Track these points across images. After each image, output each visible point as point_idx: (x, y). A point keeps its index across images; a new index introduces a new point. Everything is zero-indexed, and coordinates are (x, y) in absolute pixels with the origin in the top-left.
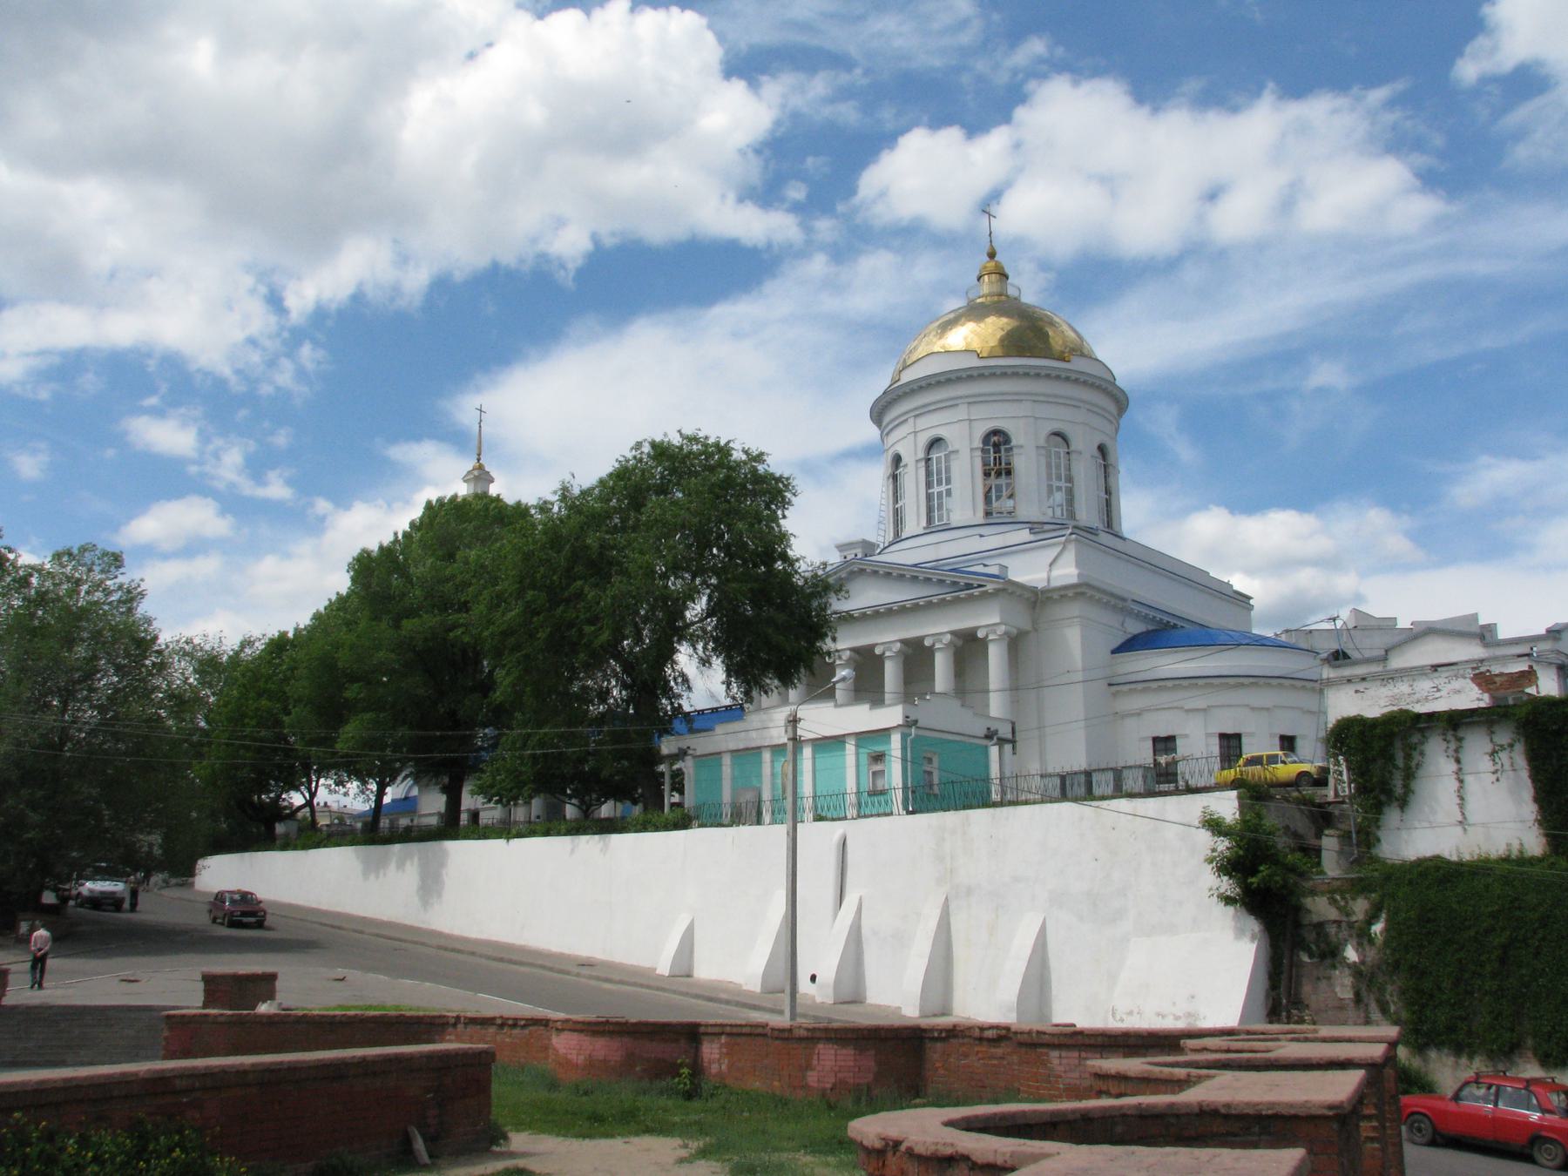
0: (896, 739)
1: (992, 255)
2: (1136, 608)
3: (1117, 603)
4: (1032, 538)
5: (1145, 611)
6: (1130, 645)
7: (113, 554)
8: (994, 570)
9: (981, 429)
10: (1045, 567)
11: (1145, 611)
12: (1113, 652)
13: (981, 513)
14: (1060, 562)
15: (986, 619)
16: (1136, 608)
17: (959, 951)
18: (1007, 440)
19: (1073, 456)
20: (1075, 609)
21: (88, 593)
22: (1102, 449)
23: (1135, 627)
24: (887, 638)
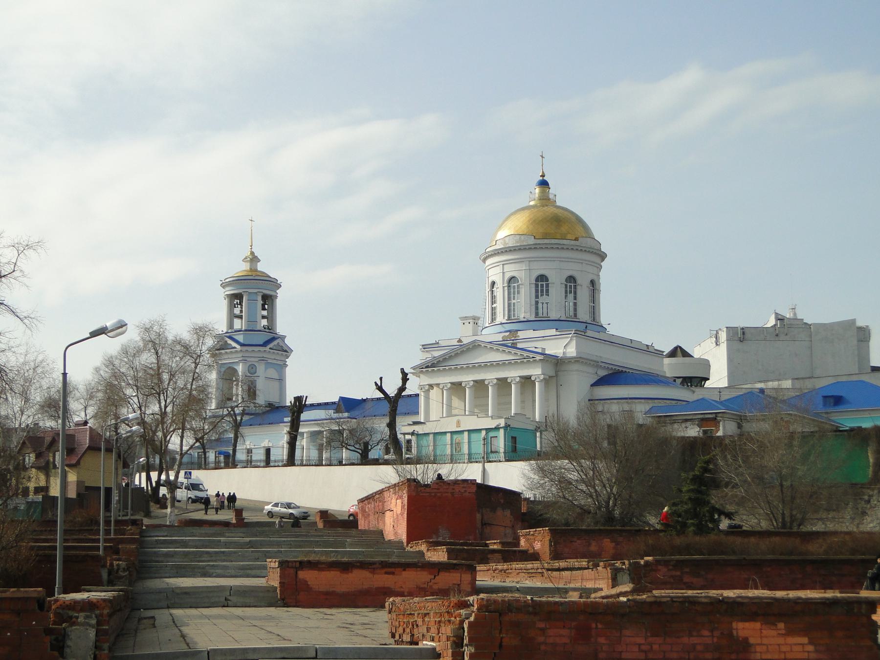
0: (502, 431)
1: (543, 176)
2: (603, 365)
3: (596, 364)
4: (558, 333)
5: (607, 366)
6: (601, 382)
7: (235, 466)
8: (539, 350)
9: (536, 274)
10: (562, 346)
11: (607, 366)
12: (592, 385)
13: (534, 316)
14: (570, 346)
15: (536, 372)
16: (603, 365)
17: (514, 210)
18: (547, 279)
19: (578, 287)
20: (575, 367)
21: (470, 615)
22: (593, 283)
23: (603, 373)
24: (490, 376)
